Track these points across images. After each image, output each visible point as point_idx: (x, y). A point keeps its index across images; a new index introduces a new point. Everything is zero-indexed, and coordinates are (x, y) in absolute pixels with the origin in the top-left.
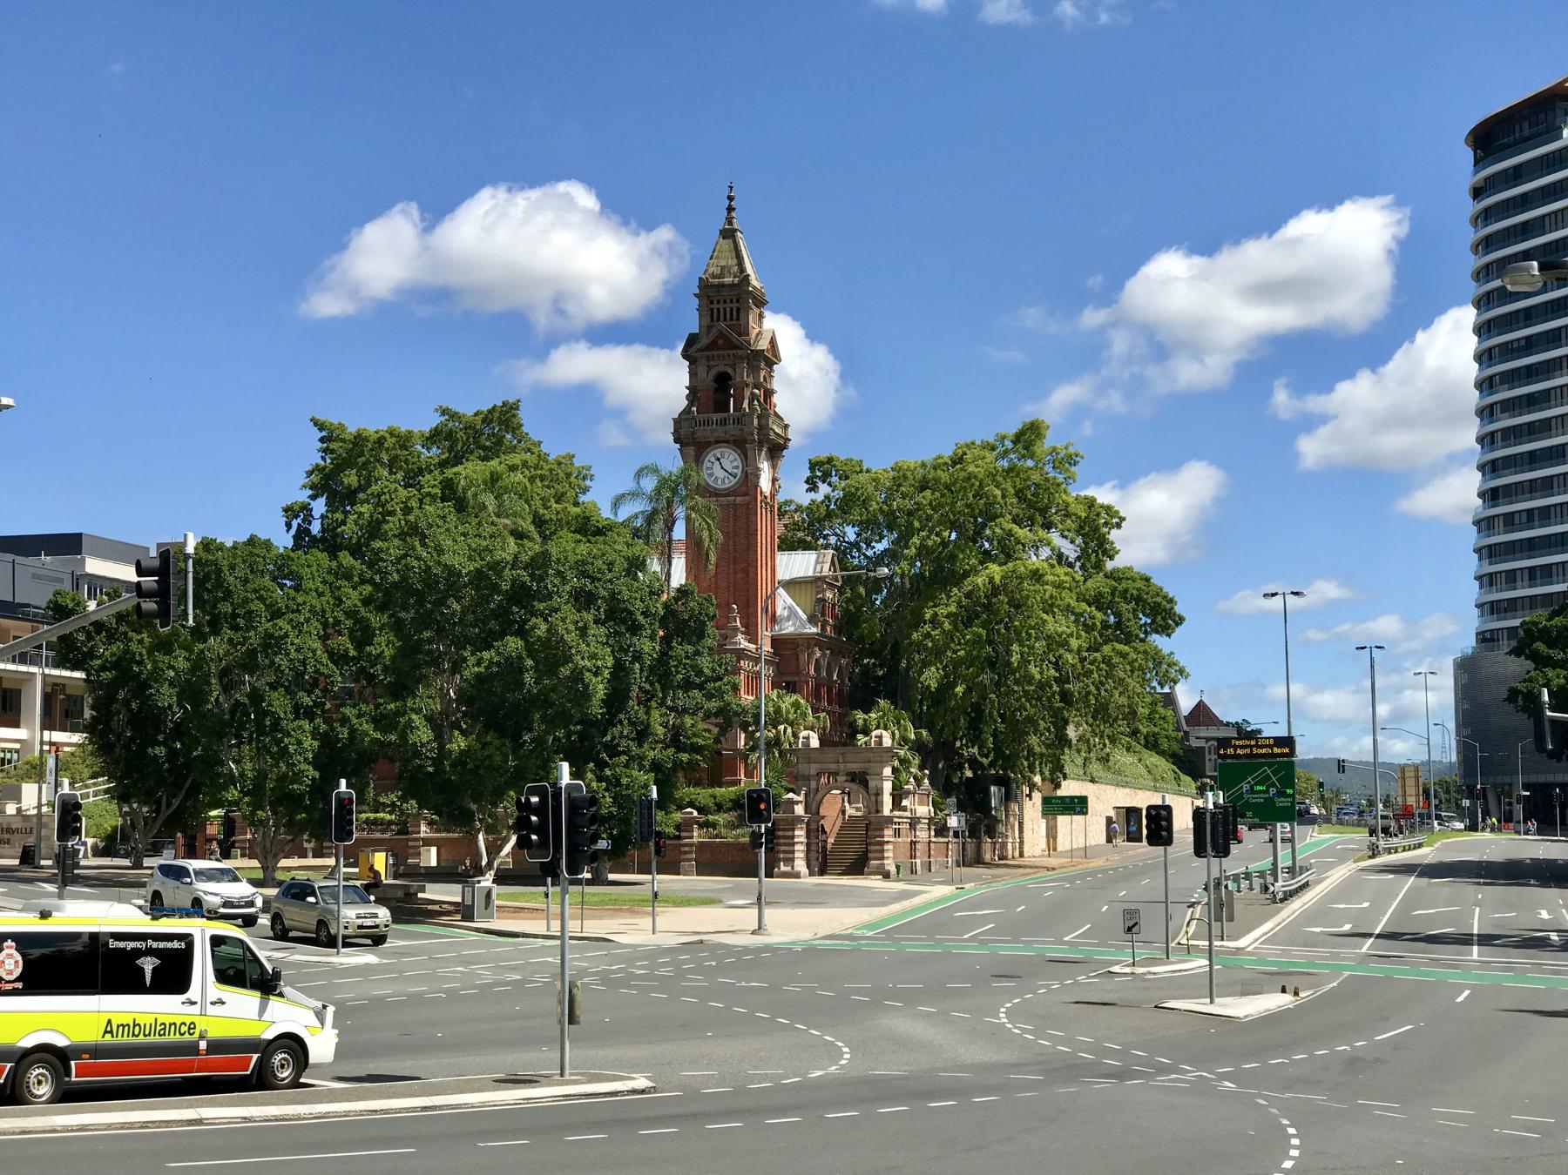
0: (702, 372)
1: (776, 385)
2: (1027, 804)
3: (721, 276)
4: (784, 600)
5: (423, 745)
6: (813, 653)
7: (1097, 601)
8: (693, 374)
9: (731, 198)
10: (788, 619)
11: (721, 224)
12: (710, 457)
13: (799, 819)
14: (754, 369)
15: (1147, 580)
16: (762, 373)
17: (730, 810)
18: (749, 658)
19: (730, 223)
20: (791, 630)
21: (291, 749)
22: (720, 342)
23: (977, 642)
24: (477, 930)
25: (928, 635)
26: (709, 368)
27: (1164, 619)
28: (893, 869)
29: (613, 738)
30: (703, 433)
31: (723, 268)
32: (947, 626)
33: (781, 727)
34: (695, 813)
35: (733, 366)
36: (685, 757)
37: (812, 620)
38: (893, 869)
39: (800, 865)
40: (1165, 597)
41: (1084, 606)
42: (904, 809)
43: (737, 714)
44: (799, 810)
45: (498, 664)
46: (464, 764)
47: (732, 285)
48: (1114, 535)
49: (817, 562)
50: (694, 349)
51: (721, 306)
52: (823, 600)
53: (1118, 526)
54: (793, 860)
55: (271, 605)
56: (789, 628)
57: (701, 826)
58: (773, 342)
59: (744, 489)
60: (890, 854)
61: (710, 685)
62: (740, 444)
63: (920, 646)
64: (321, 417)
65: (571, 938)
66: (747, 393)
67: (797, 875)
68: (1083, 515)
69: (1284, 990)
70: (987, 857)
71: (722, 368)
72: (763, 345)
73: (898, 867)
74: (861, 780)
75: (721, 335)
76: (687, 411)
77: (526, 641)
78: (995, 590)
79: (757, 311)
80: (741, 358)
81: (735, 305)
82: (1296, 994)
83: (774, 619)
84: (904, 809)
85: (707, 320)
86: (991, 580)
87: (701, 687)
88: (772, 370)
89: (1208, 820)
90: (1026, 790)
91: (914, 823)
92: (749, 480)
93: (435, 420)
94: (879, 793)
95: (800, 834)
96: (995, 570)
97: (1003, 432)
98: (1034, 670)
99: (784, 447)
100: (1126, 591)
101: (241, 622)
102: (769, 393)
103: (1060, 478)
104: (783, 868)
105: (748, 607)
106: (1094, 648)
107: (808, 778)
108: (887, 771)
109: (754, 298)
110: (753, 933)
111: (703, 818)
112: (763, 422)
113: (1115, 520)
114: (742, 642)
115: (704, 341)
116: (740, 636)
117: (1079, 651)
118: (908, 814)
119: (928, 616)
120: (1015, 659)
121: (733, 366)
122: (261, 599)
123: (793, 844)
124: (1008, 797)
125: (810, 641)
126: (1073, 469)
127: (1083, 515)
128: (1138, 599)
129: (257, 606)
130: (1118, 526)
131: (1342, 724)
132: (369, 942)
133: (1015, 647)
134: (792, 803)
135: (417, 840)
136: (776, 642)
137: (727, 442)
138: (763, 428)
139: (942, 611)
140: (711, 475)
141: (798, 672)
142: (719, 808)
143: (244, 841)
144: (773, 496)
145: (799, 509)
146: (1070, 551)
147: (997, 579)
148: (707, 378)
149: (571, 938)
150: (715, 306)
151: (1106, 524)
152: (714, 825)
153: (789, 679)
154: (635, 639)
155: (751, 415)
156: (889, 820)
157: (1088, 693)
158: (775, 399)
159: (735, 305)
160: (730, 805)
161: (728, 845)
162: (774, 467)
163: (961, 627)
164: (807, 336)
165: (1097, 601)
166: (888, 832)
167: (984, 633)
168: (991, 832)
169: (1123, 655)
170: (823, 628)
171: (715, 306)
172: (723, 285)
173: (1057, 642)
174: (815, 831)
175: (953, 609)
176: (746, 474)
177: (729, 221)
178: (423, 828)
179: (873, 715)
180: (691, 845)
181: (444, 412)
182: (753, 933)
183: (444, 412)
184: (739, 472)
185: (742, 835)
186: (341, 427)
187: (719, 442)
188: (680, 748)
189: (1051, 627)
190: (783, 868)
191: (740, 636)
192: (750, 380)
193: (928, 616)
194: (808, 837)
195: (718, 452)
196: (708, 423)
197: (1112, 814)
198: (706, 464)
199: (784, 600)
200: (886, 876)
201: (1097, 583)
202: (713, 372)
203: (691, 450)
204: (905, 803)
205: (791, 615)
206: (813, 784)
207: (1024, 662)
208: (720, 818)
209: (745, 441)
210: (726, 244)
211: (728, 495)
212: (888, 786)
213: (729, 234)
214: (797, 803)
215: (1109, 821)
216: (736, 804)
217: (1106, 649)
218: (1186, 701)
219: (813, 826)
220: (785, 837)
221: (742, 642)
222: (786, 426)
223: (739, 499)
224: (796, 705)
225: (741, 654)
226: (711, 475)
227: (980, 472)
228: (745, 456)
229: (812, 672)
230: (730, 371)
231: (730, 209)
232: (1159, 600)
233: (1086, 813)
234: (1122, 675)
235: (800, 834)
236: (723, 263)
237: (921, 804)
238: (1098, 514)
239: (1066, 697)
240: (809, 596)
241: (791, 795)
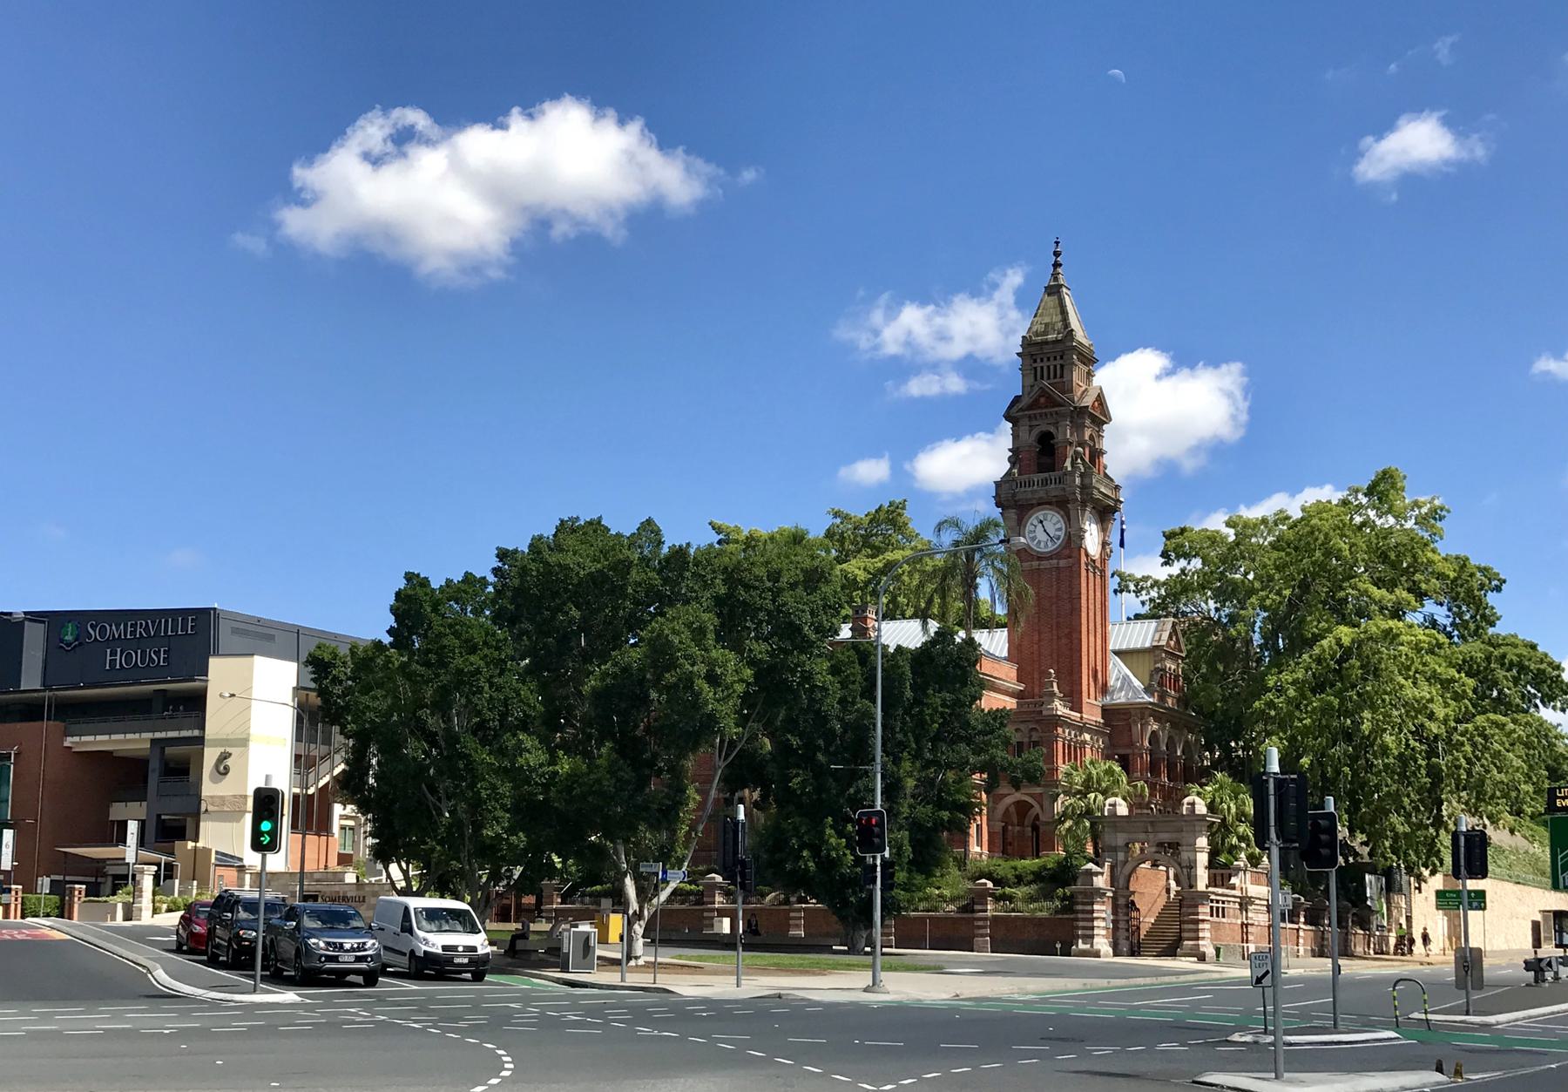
1: (1106, 444)
2: (1417, 898)
3: (1045, 333)
4: (1117, 670)
5: (532, 769)
6: (1147, 723)
7: (1468, 667)
8: (1015, 436)
9: (1057, 254)
10: (1121, 689)
11: (1047, 280)
12: (1033, 520)
13: (1099, 893)
14: (1079, 428)
15: (1533, 647)
16: (1087, 433)
17: (1029, 883)
18: (1070, 726)
19: (1056, 279)
20: (1123, 700)
21: (484, 794)
23: (1326, 710)
24: (557, 981)
25: (1271, 704)
27: (1550, 687)
28: (1210, 951)
29: (858, 791)
30: (1024, 494)
31: (1047, 325)
32: (1292, 693)
33: (1092, 796)
34: (990, 885)
35: (1056, 424)
36: (945, 815)
37: (1148, 690)
38: (1210, 951)
39: (1102, 943)
40: (1550, 664)
41: (1453, 672)
42: (1233, 887)
43: (1004, 769)
44: (1101, 882)
45: (615, 676)
46: (570, 789)
47: (1056, 341)
48: (1491, 598)
49: (1156, 631)
50: (1015, 408)
52: (1163, 670)
53: (1498, 589)
54: (1092, 937)
55: (466, 641)
56: (1120, 698)
57: (997, 899)
58: (1100, 399)
59: (1067, 552)
60: (1207, 934)
61: (979, 739)
62: (1061, 504)
63: (1262, 715)
64: (718, 522)
66: (1070, 452)
67: (1097, 954)
68: (1452, 575)
69: (1439, 1069)
70: (1359, 950)
71: (1044, 428)
72: (1088, 401)
73: (1218, 950)
74: (1172, 851)
75: (1043, 392)
76: (1009, 473)
78: (1347, 653)
79: (1086, 369)
80: (1064, 416)
82: (1458, 1073)
83: (1105, 690)
84: (1233, 887)
85: (1031, 380)
86: (1338, 642)
87: (969, 741)
88: (1100, 430)
90: (1414, 884)
91: (1245, 903)
92: (1073, 541)
93: (828, 522)
94: (1192, 866)
95: (1102, 910)
96: (1345, 633)
97: (1356, 485)
98: (1389, 739)
99: (1114, 510)
100: (1504, 656)
101: (433, 657)
102: (1096, 454)
103: (1426, 535)
104: (1081, 946)
105: (1071, 674)
106: (1468, 717)
107: (1115, 849)
108: (1202, 842)
109: (1080, 354)
110: (865, 990)
111: (999, 891)
112: (1087, 481)
113: (1495, 583)
114: (1060, 708)
115: (1026, 401)
116: (1057, 703)
117: (1445, 721)
118: (1237, 893)
119: (1271, 683)
120: (1366, 727)
122: (457, 635)
123: (1093, 920)
124: (1391, 888)
125: (1143, 711)
126: (1439, 524)
127: (1452, 575)
128: (1522, 668)
129: (450, 641)
130: (1498, 589)
132: (360, 979)
133: (1367, 714)
134: (1090, 874)
135: (713, 910)
136: (1106, 711)
137: (1050, 503)
138: (1086, 488)
139: (1286, 677)
140: (1033, 539)
141: (1131, 744)
142: (1019, 880)
143: (551, 910)
144: (1103, 561)
145: (1156, 583)
146: (1442, 615)
147: (1346, 641)
148: (1029, 438)
150: (1038, 365)
151: (1482, 587)
152: (1010, 898)
153: (1122, 752)
154: (803, 657)
155: (1072, 474)
156: (1204, 896)
157: (1458, 767)
158: (1105, 459)
160: (1031, 877)
161: (1024, 919)
162: (1104, 530)
163: (1309, 694)
165: (1468, 667)
166: (1204, 911)
167: (1336, 702)
168: (1364, 923)
169: (1501, 726)
170: (1162, 697)
171: (1038, 365)
172: (1046, 342)
173: (1421, 708)
174: (1124, 906)
175: (1300, 675)
176: (1069, 536)
177: (1055, 276)
178: (718, 898)
179: (1208, 788)
180: (985, 919)
181: (836, 514)
182: (865, 990)
183: (836, 514)
184: (1062, 534)
185: (1043, 910)
186: (738, 530)
187: (1041, 504)
188: (940, 804)
189: (1410, 692)
190: (1081, 946)
191: (1057, 703)
192: (1075, 439)
193: (1271, 683)
194: (1115, 912)
195: (1040, 515)
196: (1030, 483)
197: (1539, 918)
198: (1029, 527)
199: (1117, 670)
200: (1202, 958)
201: (1474, 649)
202: (1036, 431)
203: (1012, 513)
204: (1233, 880)
205: (1128, 685)
206: (1121, 856)
207: (1378, 731)
208: (1020, 892)
209: (1068, 502)
210: (1051, 301)
211: (1051, 558)
212: (1202, 859)
213: (1054, 290)
214: (1097, 874)
215: (1536, 926)
216: (1038, 876)
217: (1480, 719)
219: (1122, 901)
220: (1083, 912)
221: (1060, 708)
222: (1117, 488)
223: (1063, 563)
224: (1110, 772)
225: (1057, 721)
226: (1033, 539)
227: (1326, 526)
228: (1067, 518)
229: (1146, 743)
230: (1052, 429)
231: (1056, 265)
232: (1543, 666)
233: (1484, 909)
234: (1497, 746)
235: (1102, 910)
236: (1047, 320)
237: (1256, 882)
238: (1472, 575)
239: (1434, 772)
240: (1147, 665)
241: (1090, 866)
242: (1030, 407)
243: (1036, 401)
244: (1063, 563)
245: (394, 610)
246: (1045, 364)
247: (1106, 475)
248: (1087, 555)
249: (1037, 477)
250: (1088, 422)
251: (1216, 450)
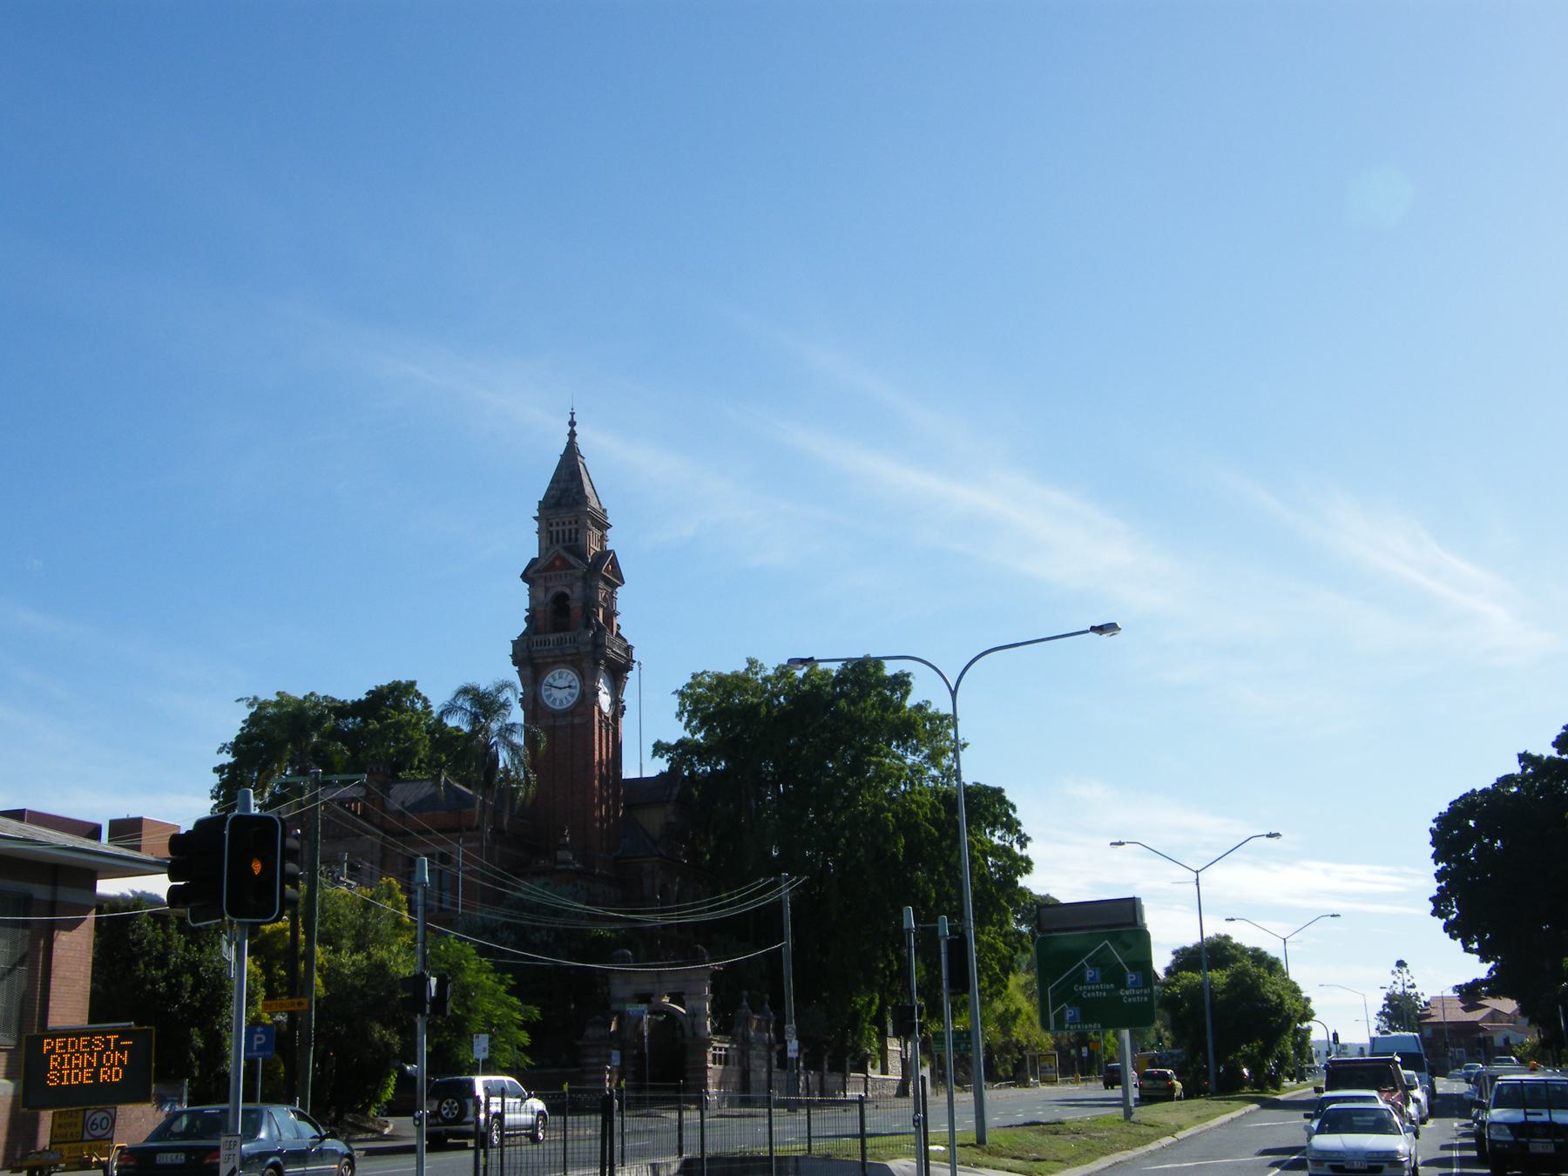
0: (541, 595)
22: (557, 563)
26: (547, 589)
51: (560, 528)
62: (575, 663)
65: (962, 1145)
71: (560, 589)
75: (559, 557)
77: (355, 755)
81: (574, 526)
89: (185, 1097)
121: (570, 586)
131: (636, 1133)
137: (565, 662)
149: (962, 1145)
150: (554, 528)
159: (574, 526)
164: (1184, 949)
171: (554, 528)
176: (583, 694)
202: (550, 595)
203: (528, 671)
218: (910, 702)
228: (582, 676)
230: (567, 591)
231: (572, 424)
242: (547, 569)
243: (553, 562)
244: (576, 721)
245: (1453, 937)
246: (567, 527)
247: (618, 635)
248: (601, 712)
249: (552, 637)
250: (601, 584)
251: (61, 929)
